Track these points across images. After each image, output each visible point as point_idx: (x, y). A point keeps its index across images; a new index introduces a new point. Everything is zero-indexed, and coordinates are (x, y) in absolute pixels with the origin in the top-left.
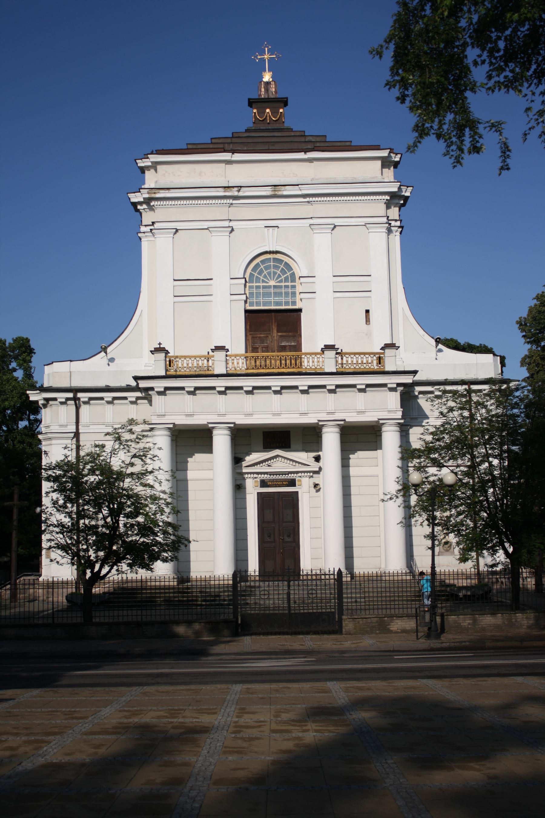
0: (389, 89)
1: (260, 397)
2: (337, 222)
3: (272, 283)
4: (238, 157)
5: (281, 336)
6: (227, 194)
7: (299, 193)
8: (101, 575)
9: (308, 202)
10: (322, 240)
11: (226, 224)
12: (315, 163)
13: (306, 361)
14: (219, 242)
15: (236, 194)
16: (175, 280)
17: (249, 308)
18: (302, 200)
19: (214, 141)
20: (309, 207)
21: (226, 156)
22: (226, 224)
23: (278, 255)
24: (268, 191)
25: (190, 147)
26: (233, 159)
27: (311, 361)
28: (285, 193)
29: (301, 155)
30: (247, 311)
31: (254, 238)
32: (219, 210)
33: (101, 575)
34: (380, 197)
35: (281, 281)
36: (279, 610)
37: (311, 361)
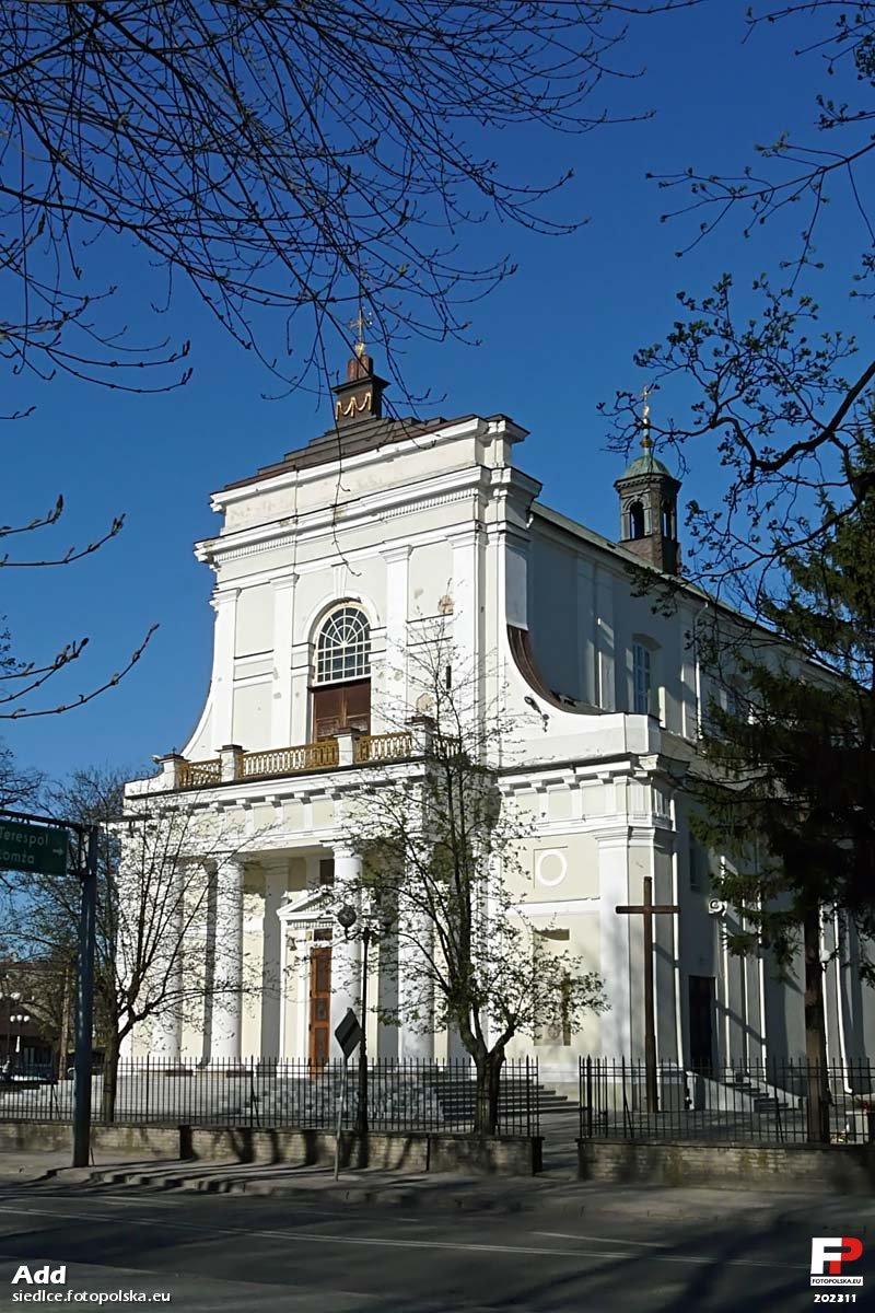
0: (864, 264)
1: (236, 815)
2: (413, 541)
3: (344, 644)
4: (305, 474)
5: (351, 720)
6: (285, 529)
7: (363, 509)
8: (489, 1051)
9: (381, 520)
10: (397, 571)
11: (290, 570)
12: (396, 460)
13: (373, 747)
14: (283, 595)
15: (294, 527)
16: (235, 658)
17: (315, 683)
18: (370, 518)
19: (288, 458)
20: (385, 527)
21: (291, 477)
22: (290, 570)
23: (351, 603)
24: (328, 516)
25: (261, 472)
26: (300, 479)
27: (380, 749)
28: (349, 513)
29: (373, 455)
30: (311, 689)
31: (324, 586)
32: (279, 555)
33: (489, 1051)
34: (465, 493)
35: (353, 641)
36: (842, 1068)
37: (380, 749)
